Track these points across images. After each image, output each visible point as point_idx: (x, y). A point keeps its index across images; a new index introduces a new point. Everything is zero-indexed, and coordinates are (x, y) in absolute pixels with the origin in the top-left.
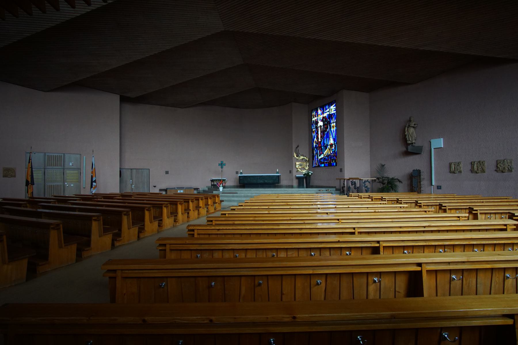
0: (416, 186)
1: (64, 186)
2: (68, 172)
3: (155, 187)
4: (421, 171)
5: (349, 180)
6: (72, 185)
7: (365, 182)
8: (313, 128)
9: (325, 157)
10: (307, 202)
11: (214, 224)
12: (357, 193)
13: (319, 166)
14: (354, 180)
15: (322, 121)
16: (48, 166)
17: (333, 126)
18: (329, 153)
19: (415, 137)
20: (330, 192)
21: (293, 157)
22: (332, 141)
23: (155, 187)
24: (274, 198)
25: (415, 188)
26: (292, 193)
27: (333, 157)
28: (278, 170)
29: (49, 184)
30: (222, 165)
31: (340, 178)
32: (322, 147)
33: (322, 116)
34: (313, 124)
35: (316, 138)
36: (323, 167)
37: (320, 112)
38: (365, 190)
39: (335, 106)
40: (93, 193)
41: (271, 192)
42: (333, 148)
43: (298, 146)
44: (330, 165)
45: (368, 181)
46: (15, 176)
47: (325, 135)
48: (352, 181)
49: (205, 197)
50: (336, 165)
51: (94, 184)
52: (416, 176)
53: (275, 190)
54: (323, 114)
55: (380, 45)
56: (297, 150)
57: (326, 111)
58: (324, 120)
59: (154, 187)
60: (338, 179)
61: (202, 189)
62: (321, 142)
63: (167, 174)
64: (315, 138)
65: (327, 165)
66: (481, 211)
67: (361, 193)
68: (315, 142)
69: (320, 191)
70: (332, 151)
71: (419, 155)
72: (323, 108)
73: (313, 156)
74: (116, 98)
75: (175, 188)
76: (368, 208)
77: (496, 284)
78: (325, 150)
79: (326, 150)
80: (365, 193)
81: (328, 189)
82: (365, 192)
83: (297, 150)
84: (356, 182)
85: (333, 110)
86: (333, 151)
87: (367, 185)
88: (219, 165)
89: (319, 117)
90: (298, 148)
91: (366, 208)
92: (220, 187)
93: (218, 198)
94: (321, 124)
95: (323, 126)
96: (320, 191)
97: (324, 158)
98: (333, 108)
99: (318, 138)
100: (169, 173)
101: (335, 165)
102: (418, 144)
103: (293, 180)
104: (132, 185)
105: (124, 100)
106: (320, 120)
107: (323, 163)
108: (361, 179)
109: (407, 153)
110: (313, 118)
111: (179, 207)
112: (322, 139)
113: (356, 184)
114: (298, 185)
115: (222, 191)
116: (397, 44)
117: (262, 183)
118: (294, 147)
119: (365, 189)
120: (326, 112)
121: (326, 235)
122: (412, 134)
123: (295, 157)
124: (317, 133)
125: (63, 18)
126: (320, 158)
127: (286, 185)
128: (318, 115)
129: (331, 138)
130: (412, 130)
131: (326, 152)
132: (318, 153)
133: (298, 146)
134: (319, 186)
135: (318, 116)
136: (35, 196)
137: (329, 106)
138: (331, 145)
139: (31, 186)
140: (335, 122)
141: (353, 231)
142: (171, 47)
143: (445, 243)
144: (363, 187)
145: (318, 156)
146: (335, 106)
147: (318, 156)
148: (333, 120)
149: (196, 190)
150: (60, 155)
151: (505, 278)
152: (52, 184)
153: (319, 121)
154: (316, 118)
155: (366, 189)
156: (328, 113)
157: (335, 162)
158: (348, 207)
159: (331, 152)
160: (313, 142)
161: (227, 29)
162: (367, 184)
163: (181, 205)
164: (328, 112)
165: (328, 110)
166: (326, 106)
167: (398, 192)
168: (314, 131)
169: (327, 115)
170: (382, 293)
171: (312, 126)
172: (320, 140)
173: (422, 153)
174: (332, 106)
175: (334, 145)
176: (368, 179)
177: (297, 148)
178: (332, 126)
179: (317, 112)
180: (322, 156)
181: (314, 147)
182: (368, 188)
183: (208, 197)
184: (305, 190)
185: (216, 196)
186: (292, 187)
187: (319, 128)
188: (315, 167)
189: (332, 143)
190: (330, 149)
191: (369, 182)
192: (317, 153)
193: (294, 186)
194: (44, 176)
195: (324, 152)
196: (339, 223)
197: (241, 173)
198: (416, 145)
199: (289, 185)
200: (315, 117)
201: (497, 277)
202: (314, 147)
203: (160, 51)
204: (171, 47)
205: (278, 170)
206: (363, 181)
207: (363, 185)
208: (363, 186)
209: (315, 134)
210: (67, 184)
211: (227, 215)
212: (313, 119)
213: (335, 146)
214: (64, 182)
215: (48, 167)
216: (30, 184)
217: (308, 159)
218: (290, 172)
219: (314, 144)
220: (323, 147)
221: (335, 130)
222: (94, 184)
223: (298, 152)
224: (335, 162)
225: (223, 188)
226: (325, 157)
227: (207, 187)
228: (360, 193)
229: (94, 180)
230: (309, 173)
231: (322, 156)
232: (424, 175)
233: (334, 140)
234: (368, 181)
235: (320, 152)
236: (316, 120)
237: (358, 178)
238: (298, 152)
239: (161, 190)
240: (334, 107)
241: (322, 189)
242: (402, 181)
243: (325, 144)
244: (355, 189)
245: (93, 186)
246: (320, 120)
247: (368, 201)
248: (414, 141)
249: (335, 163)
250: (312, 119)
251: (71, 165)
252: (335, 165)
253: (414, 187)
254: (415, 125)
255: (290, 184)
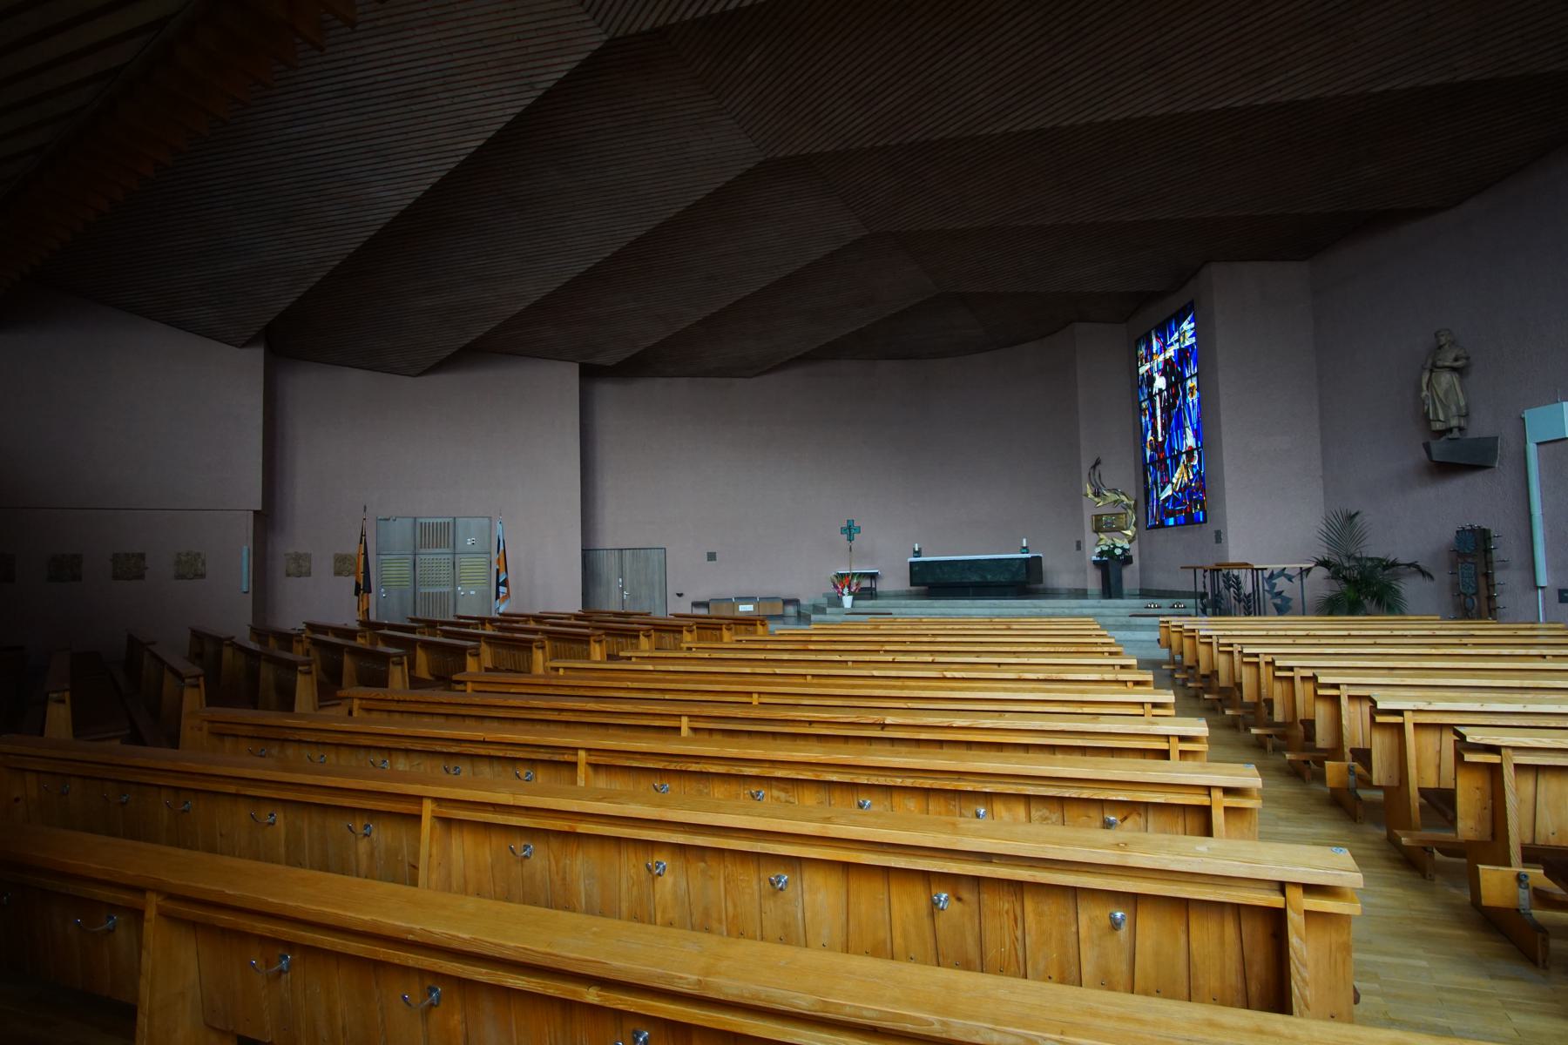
0: (1471, 591)
1: (455, 594)
2: (464, 561)
3: (680, 595)
4: (1492, 534)
5: (1218, 570)
6: (473, 593)
7: (1272, 576)
8: (1142, 399)
9: (1177, 493)
10: (905, 642)
11: (755, 703)
12: (1246, 615)
13: (1162, 525)
14: (1236, 572)
15: (1163, 373)
16: (421, 548)
17: (1191, 389)
18: (1186, 479)
19: (1462, 403)
20: (1183, 611)
21: (1084, 497)
22: (1190, 441)
23: (680, 595)
24: (867, 629)
25: (1468, 600)
26: (1053, 616)
27: (1197, 494)
28: (1024, 541)
29: (423, 591)
30: (850, 530)
31: (1196, 565)
32: (1166, 458)
33: (1161, 358)
34: (1140, 387)
35: (1150, 432)
36: (1171, 526)
37: (1156, 345)
38: (1275, 605)
39: (1193, 320)
40: (501, 610)
41: (987, 611)
42: (1195, 462)
43: (1098, 463)
44: (1191, 520)
45: (1286, 572)
46: (308, 574)
47: (1173, 421)
48: (1228, 573)
49: (697, 623)
50: (1205, 521)
51: (502, 589)
52: (1468, 551)
53: (1004, 605)
54: (1165, 350)
55: (1262, 102)
56: (1097, 474)
57: (1172, 340)
58: (1168, 369)
59: (678, 598)
60: (1192, 567)
61: (812, 603)
62: (1163, 442)
63: (715, 557)
64: (1148, 430)
65: (1182, 521)
66: (1351, 688)
67: (1260, 614)
68: (1148, 444)
69: (1147, 607)
70: (1192, 471)
71: (1487, 471)
72: (1164, 329)
73: (1147, 493)
74: (567, 376)
75: (731, 599)
76: (999, 664)
77: (633, 885)
78: (1176, 470)
79: (1179, 470)
80: (1273, 615)
81: (1176, 600)
82: (1276, 613)
83: (1097, 474)
84: (1242, 579)
85: (1188, 334)
86: (1195, 470)
87: (1280, 590)
88: (843, 531)
89: (1154, 364)
90: (1098, 468)
91: (996, 667)
92: (844, 595)
93: (765, 627)
94: (1160, 383)
95: (1167, 389)
96: (1148, 610)
97: (1174, 497)
98: (1187, 326)
99: (1155, 433)
100: (706, 556)
101: (1201, 519)
102: (1480, 427)
103: (1085, 571)
104: (622, 589)
105: (590, 374)
106: (1158, 371)
107: (1172, 514)
108: (1255, 567)
109: (1444, 469)
110: (1142, 365)
111: (594, 648)
112: (1165, 434)
113: (1243, 584)
114: (1101, 587)
115: (852, 606)
116: (1280, 91)
117: (976, 582)
118: (1086, 466)
119: (1273, 601)
120: (1171, 344)
121: (1028, 753)
122: (1446, 393)
123: (1090, 496)
124: (1153, 416)
125: (384, 216)
126: (1163, 496)
127: (1067, 587)
128: (1152, 354)
129: (1187, 429)
130: (1445, 379)
131: (1176, 475)
132: (1159, 481)
133: (1098, 463)
134: (1165, 591)
135: (1152, 359)
136: (373, 617)
137: (1179, 324)
138: (1190, 453)
139: (365, 594)
140: (1197, 374)
141: (1163, 746)
142: (645, 229)
143: (1023, 790)
144: (1266, 593)
145: (1160, 489)
146: (1193, 320)
147: (1160, 489)
148: (1191, 370)
149: (794, 605)
150: (447, 520)
151: (653, 874)
152: (431, 591)
153: (1156, 375)
154: (1148, 366)
155: (1278, 601)
156: (1176, 346)
157: (1203, 508)
158: (893, 662)
159: (1191, 477)
160: (1145, 446)
161: (769, 156)
162: (1281, 583)
163: (600, 646)
164: (1176, 341)
165: (1176, 335)
166: (1168, 321)
167: (1406, 611)
168: (1145, 410)
169: (1175, 350)
170: (1027, 952)
171: (1140, 394)
172: (1160, 439)
173: (1497, 466)
174: (1186, 322)
175: (1196, 453)
176: (1284, 566)
177: (1094, 467)
178: (1188, 388)
179: (1149, 347)
180: (1168, 491)
181: (1148, 461)
182: (1287, 600)
183: (721, 625)
184: (1099, 605)
185: (758, 622)
186: (1082, 594)
187: (1158, 398)
188: (1152, 527)
189: (1190, 447)
190: (1186, 467)
191: (1290, 578)
192: (1155, 482)
193: (1089, 593)
194: (413, 572)
195: (1173, 476)
196: (1143, 715)
197: (918, 553)
198: (1472, 434)
199: (1076, 590)
200: (1146, 362)
201: (634, 866)
202: (1148, 461)
203: (624, 244)
204: (645, 229)
205: (1024, 541)
206: (1267, 574)
207: (1267, 588)
208: (1264, 590)
209: (1148, 418)
210: (461, 591)
211: (561, 672)
212: (1142, 370)
213: (1199, 454)
214: (455, 586)
215: (423, 551)
216: (362, 592)
217: (1132, 502)
218: (1079, 546)
219: (1148, 453)
220: (1168, 461)
221: (1196, 401)
222: (502, 589)
223: (1098, 481)
224: (1200, 509)
225: (854, 599)
226: (1177, 493)
227: (824, 595)
228: (1255, 615)
229: (501, 580)
230: (1115, 547)
231: (1168, 491)
232: (1506, 549)
233: (1197, 435)
234: (1286, 572)
235: (1162, 477)
236: (1147, 371)
237: (1247, 564)
238: (1098, 481)
239: (696, 605)
240: (1190, 323)
241: (1156, 601)
242: (1432, 573)
243: (1174, 449)
244: (1239, 601)
245: (501, 595)
246: (1158, 371)
247: (911, 642)
248: (1454, 422)
249: (1201, 513)
250: (1138, 368)
251: (469, 543)
252: (1201, 519)
253: (1465, 595)
254: (1456, 360)
255: (1079, 586)
